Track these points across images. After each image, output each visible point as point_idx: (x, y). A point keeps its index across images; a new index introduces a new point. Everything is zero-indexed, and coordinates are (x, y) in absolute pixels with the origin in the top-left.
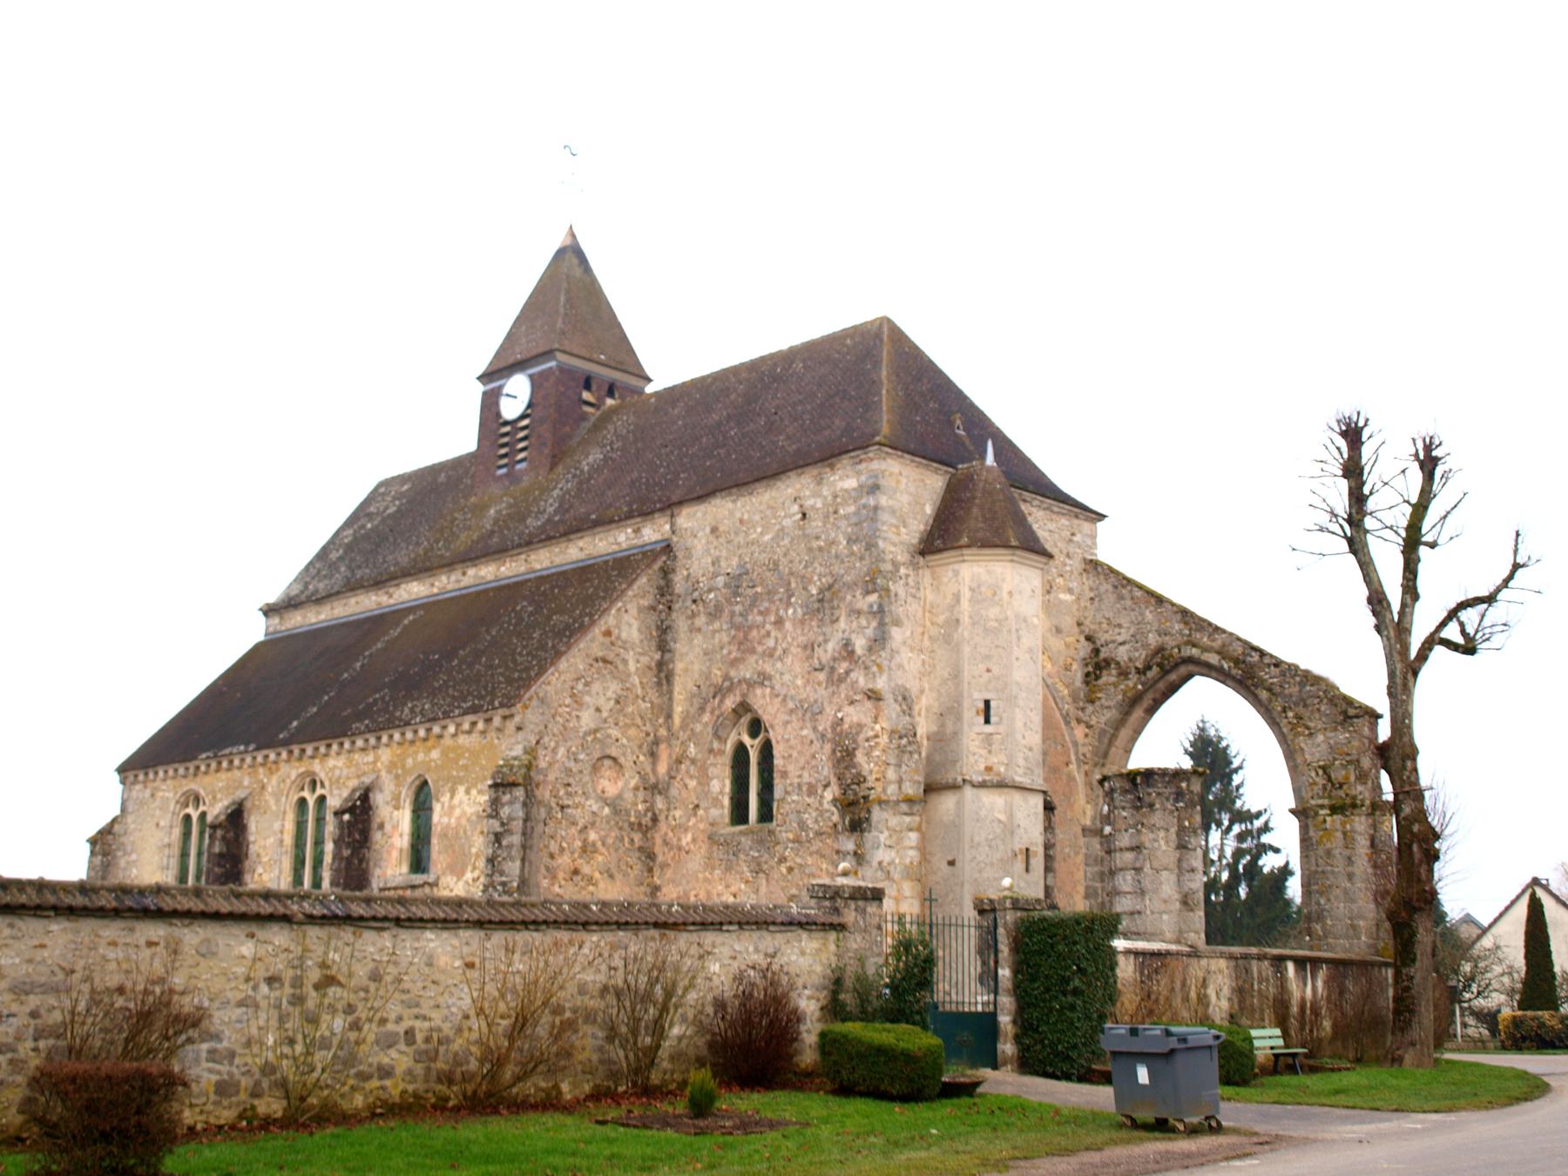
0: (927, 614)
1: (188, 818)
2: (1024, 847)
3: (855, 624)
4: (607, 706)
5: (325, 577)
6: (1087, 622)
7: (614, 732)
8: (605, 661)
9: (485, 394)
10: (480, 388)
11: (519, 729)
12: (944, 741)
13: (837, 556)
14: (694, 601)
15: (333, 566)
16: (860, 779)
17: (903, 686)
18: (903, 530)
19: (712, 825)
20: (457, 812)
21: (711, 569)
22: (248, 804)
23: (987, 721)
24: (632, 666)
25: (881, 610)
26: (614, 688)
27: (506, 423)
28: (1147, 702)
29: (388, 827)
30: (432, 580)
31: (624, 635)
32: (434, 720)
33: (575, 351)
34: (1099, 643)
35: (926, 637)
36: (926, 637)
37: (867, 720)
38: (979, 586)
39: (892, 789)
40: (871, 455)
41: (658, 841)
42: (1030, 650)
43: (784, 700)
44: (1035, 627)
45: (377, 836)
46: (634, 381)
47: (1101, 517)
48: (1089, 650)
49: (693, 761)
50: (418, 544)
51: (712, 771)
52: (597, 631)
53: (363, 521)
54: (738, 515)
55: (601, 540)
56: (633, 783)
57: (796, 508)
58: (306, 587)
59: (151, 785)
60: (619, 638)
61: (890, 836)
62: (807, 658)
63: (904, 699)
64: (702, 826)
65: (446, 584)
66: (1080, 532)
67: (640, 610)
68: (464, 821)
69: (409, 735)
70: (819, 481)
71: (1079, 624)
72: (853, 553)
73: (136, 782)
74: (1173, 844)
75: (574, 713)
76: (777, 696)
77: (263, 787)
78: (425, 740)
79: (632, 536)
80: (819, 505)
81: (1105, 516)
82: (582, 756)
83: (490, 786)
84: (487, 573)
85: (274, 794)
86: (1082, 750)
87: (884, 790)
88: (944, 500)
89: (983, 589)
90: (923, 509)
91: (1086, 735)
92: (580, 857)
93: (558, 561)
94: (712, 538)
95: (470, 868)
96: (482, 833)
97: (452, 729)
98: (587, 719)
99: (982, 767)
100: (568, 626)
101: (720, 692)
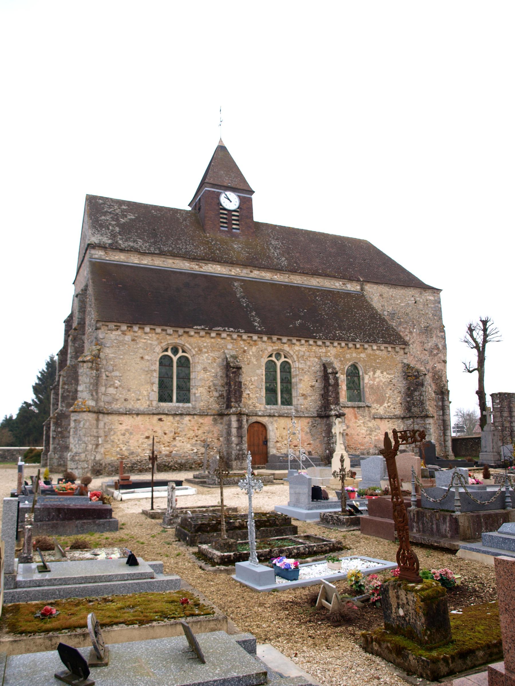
20: (377, 380)
30: (230, 268)
54: (391, 294)
57: (413, 299)
80: (421, 301)
93: (306, 283)
94: (380, 298)
95: (386, 402)
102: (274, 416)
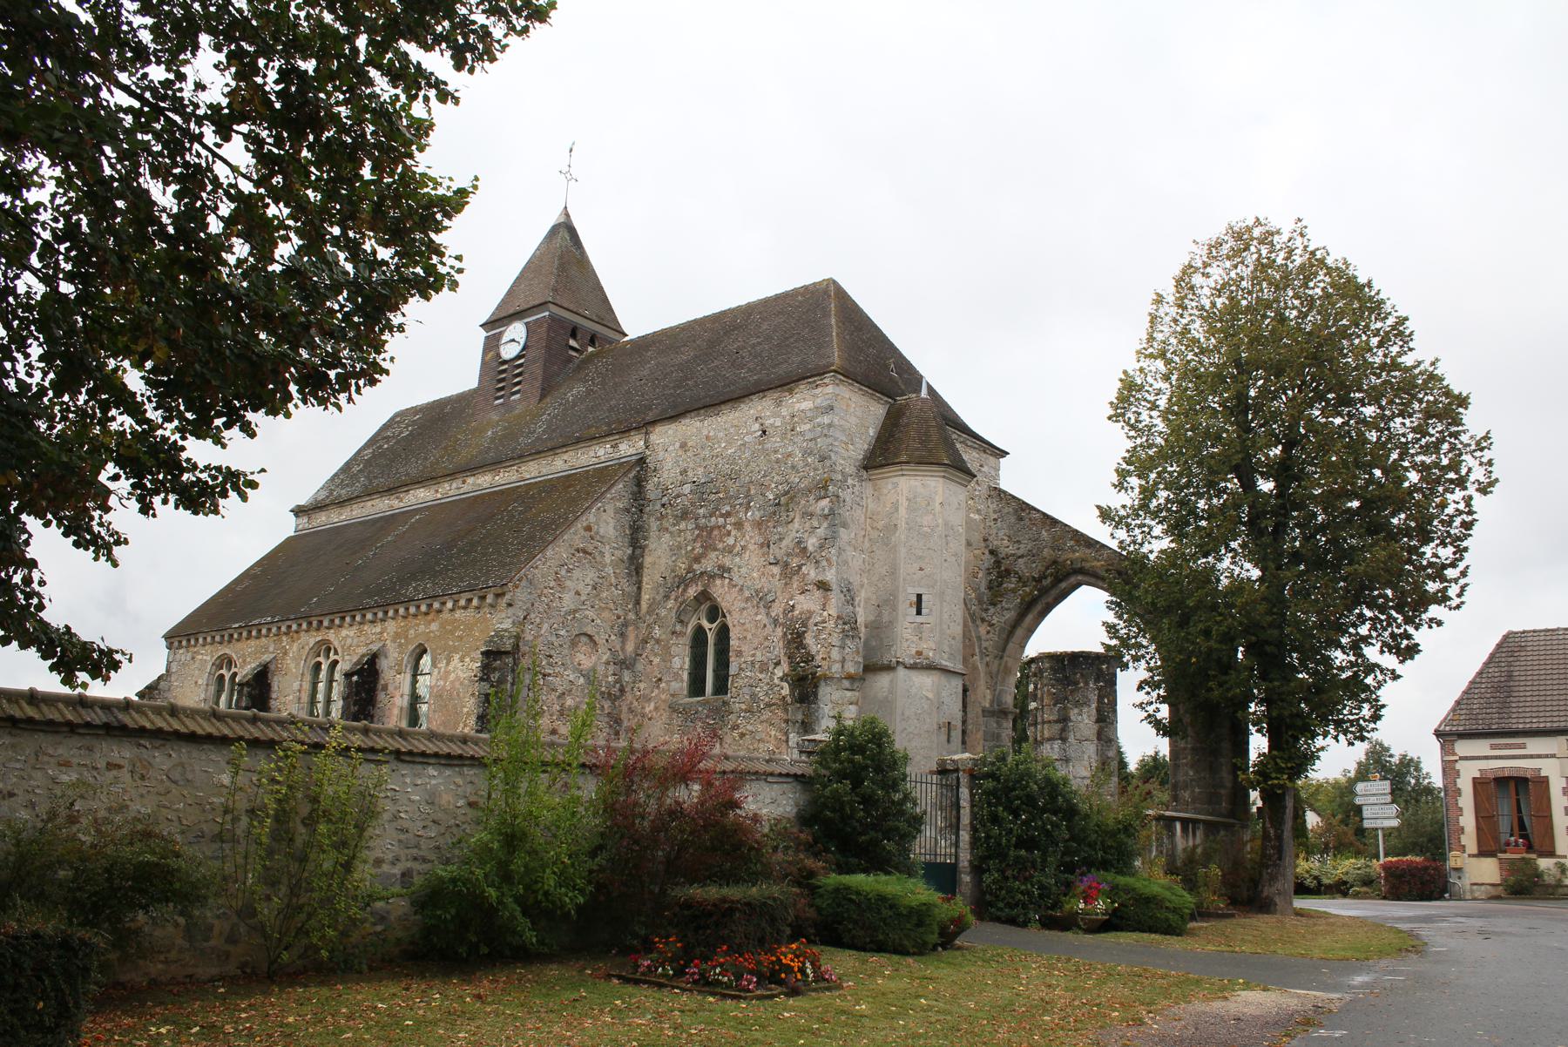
1: (222, 677)
4: (585, 591)
5: (347, 485)
6: (991, 538)
7: (591, 614)
8: (585, 552)
9: (487, 338)
10: (483, 334)
11: (510, 605)
12: (880, 629)
13: (793, 467)
14: (663, 505)
15: (354, 477)
16: (809, 658)
19: (673, 695)
20: (452, 677)
21: (680, 478)
22: (272, 667)
23: (919, 612)
24: (608, 559)
25: (832, 512)
26: (591, 576)
27: (505, 362)
28: (1039, 607)
29: (391, 688)
30: (435, 487)
31: (602, 531)
32: (435, 597)
33: (565, 305)
37: (816, 607)
38: (915, 497)
39: (836, 668)
41: (625, 709)
43: (741, 590)
44: (960, 535)
45: (381, 696)
46: (611, 334)
47: (1004, 453)
49: (658, 641)
50: (426, 459)
51: (674, 650)
52: (579, 525)
53: (381, 443)
54: (705, 432)
55: (583, 454)
56: (605, 658)
57: (757, 426)
58: (331, 494)
59: (192, 649)
60: (597, 533)
62: (763, 555)
64: (663, 697)
65: (449, 490)
67: (617, 511)
68: (457, 685)
69: (412, 610)
70: (779, 403)
71: (985, 540)
73: (180, 647)
74: (1094, 719)
75: (557, 595)
76: (735, 586)
77: (285, 653)
78: (426, 614)
79: (611, 450)
82: (562, 633)
83: (482, 653)
84: (484, 482)
85: (294, 658)
86: (985, 644)
87: (829, 668)
91: (988, 632)
92: (558, 719)
94: (680, 453)
96: (473, 694)
97: (450, 605)
98: (568, 601)
99: (913, 652)
100: (553, 522)
101: (683, 582)
102: (249, 742)
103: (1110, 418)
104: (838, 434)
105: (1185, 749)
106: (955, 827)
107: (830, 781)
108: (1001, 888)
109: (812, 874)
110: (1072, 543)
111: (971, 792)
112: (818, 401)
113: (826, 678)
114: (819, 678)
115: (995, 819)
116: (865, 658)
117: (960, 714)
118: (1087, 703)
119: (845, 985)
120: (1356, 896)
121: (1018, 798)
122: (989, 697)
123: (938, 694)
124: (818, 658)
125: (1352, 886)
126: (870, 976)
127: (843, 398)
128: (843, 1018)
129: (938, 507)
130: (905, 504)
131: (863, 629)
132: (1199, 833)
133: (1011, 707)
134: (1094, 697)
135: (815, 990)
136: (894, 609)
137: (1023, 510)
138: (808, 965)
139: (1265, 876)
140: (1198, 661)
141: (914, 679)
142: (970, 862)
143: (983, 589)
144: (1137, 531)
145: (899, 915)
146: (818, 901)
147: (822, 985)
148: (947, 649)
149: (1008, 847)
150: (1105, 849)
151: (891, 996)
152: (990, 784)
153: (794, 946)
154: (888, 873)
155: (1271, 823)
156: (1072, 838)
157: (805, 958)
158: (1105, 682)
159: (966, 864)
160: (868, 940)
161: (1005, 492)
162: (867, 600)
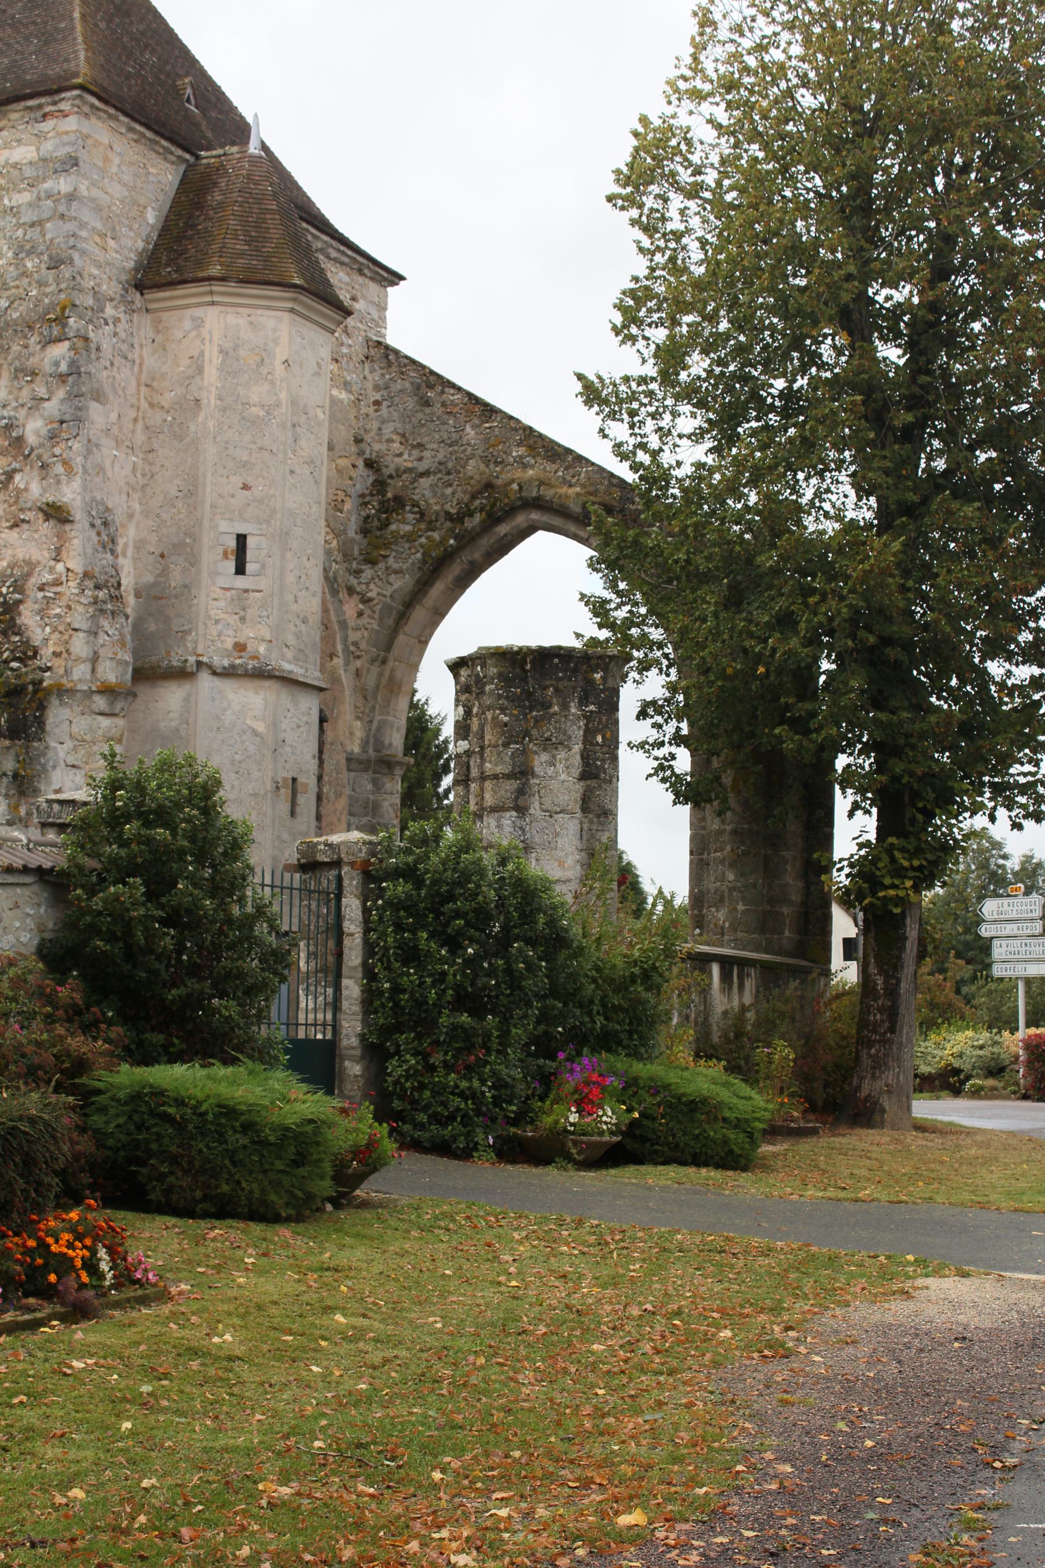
0: (143, 389)
2: (290, 776)
3: (25, 393)
6: (368, 438)
17: (102, 502)
18: (112, 243)
23: (240, 570)
25: (75, 371)
28: (456, 569)
34: (386, 472)
35: (140, 426)
36: (140, 426)
38: (236, 348)
39: (81, 672)
40: (64, 106)
42: (311, 462)
44: (319, 424)
47: (395, 278)
48: (371, 480)
61: (75, 749)
63: (105, 524)
66: (363, 297)
71: (358, 441)
72: (24, 274)
74: (576, 772)
81: (402, 278)
86: (353, 636)
88: (176, 202)
89: (242, 352)
90: (142, 214)
91: (360, 614)
99: (229, 643)
103: (610, 199)
104: (87, 215)
105: (721, 832)
106: (335, 973)
107: (102, 880)
108: (422, 1087)
109: (80, 1065)
110: (522, 451)
111: (364, 904)
112: (48, 147)
113: (61, 691)
114: (48, 692)
115: (411, 955)
116: (135, 653)
117: (313, 765)
118: (564, 744)
119: (173, 1290)
120: (977, 1094)
121: (458, 914)
122: (359, 734)
123: (275, 725)
124: (46, 652)
125: (968, 1078)
126: (218, 1268)
127: (97, 144)
128: (195, 1365)
129: (279, 368)
130: (217, 360)
131: (131, 600)
132: (750, 984)
133: (400, 754)
134: (577, 732)
135: (117, 1305)
136: (193, 561)
137: (431, 387)
138: (102, 1253)
139: (866, 1061)
140: (767, 675)
141: (231, 696)
142: (362, 1037)
143: (351, 534)
144: (650, 425)
145: (265, 1143)
146: (97, 1120)
147: (131, 1292)
148: (291, 640)
149: (438, 1006)
150: (608, 1012)
151: (273, 1310)
152: (401, 889)
153: (74, 1215)
154: (229, 1061)
155: (879, 964)
156: (554, 992)
157: (96, 1238)
158: (600, 705)
159: (354, 1041)
160: (198, 1194)
161: (396, 352)
162: (140, 544)
